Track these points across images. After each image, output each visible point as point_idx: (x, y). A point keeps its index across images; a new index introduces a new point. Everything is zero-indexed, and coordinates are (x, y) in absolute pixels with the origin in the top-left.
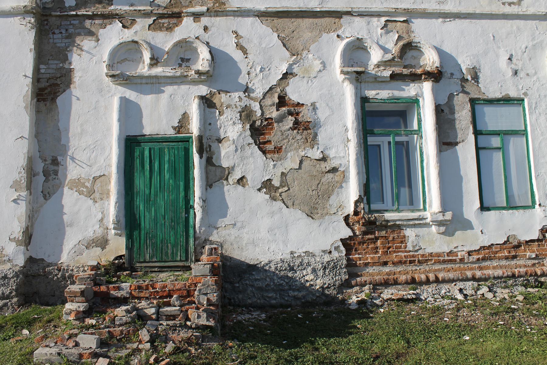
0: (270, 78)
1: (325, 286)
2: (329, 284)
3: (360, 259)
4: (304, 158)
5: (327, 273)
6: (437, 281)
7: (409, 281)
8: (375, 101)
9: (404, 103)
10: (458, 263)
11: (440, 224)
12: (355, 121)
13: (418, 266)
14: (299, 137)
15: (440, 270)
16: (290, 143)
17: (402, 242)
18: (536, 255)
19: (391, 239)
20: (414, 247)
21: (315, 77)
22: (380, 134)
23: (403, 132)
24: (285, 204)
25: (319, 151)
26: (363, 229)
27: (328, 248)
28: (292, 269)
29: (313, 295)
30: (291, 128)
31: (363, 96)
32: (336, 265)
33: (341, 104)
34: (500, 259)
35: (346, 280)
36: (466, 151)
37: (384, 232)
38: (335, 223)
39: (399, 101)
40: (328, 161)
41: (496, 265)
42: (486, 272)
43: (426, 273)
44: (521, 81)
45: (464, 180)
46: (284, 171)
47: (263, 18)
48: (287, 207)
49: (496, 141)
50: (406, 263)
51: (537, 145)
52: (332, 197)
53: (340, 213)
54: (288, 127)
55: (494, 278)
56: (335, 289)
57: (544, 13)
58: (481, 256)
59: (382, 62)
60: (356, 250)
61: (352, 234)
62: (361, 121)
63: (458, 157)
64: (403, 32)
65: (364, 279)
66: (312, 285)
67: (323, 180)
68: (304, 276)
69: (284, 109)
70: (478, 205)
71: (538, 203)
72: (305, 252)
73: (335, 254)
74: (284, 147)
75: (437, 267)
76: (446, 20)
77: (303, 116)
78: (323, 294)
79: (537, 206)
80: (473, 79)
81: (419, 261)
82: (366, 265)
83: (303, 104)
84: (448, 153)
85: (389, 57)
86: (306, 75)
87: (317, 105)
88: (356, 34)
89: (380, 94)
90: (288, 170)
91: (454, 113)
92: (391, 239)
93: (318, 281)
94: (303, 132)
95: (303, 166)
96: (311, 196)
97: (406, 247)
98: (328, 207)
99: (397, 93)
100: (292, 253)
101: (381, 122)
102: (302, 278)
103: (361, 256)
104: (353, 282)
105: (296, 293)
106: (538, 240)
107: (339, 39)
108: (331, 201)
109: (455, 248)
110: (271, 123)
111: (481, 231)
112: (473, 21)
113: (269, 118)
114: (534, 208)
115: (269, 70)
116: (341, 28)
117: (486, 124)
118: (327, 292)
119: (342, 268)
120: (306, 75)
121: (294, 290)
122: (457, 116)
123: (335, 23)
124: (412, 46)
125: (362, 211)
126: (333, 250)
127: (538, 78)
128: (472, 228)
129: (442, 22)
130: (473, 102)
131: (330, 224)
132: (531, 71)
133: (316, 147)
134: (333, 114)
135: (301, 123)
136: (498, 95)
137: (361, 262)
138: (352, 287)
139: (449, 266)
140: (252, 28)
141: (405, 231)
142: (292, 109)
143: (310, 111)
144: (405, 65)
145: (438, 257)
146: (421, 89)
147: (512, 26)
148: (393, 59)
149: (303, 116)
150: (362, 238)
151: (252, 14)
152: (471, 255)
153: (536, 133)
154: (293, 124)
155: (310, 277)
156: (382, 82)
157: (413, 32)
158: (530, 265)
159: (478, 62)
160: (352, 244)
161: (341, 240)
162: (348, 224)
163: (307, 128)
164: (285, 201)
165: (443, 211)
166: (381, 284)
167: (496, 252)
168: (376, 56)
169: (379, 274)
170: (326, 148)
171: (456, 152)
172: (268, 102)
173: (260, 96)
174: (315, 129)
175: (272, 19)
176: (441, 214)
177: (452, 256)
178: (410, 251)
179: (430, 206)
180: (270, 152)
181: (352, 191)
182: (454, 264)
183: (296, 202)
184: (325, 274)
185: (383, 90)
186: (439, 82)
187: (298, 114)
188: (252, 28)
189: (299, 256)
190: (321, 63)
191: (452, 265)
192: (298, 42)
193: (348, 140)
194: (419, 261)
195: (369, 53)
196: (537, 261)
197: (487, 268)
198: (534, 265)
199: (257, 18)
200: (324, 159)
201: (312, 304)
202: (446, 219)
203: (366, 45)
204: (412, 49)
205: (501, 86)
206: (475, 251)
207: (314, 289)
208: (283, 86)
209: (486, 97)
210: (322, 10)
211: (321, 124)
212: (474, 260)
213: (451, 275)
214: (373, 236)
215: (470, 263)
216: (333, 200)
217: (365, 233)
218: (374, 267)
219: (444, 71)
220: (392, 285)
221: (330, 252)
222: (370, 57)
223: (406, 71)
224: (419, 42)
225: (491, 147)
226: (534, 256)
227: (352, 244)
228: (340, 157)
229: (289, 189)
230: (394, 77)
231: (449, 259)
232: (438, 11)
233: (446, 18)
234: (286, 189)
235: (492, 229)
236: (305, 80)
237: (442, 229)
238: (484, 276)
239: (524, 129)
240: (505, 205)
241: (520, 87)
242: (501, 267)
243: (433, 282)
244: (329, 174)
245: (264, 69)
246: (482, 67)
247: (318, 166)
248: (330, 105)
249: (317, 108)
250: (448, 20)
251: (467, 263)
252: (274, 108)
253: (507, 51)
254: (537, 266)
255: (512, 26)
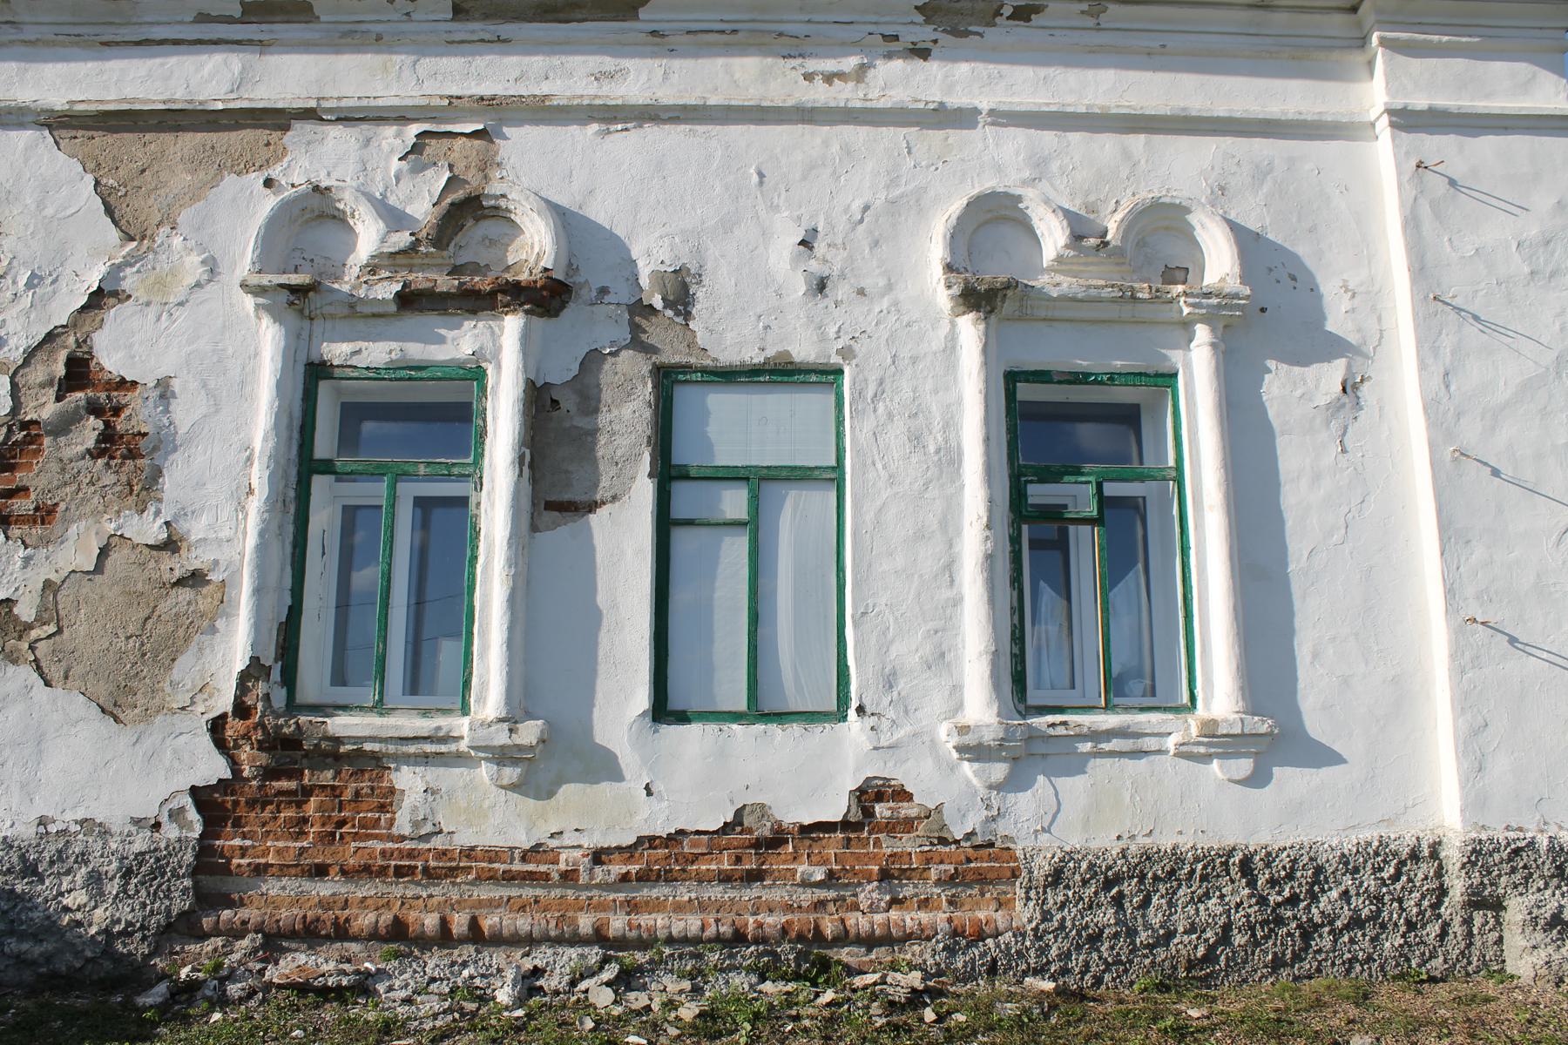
0: (54, 305)
1: (117, 929)
2: (129, 924)
3: (244, 851)
4: (114, 541)
5: (131, 889)
6: (475, 935)
7: (383, 931)
8: (350, 373)
9: (440, 379)
10: (554, 886)
11: (502, 756)
12: (272, 435)
13: (426, 887)
14: (109, 478)
15: (492, 904)
16: (81, 495)
17: (382, 808)
18: (831, 874)
19: (348, 795)
20: (416, 824)
21: (181, 304)
22: (352, 473)
23: (422, 470)
24: (42, 675)
25: (160, 521)
26: (263, 759)
27: (150, 812)
28: (30, 870)
29: (78, 954)
30: (88, 451)
31: (315, 358)
32: (162, 867)
33: (244, 385)
34: (701, 879)
35: (182, 914)
36: (622, 534)
37: (329, 774)
38: (183, 738)
39: (424, 374)
40: (183, 552)
41: (686, 898)
42: (645, 920)
43: (448, 911)
44: (836, 312)
45: (605, 622)
46: (53, 577)
47: (64, 133)
48: (48, 684)
49: (734, 502)
50: (386, 875)
51: (869, 517)
52: (181, 660)
53: (200, 708)
54: (80, 449)
55: (670, 940)
56: (144, 938)
57: (931, 106)
58: (634, 868)
59: (380, 255)
60: (237, 823)
61: (228, 775)
62: (296, 435)
63: (592, 549)
64: (467, 168)
65: (250, 914)
66: (79, 924)
67: (163, 607)
68: (61, 894)
69: (80, 395)
70: (642, 699)
71: (854, 704)
72: (82, 822)
73: (171, 832)
74: (62, 506)
75: (486, 892)
76: (613, 128)
77: (129, 418)
78: (108, 951)
79: (852, 713)
80: (668, 304)
81: (426, 870)
82: (260, 871)
83: (134, 383)
84: (561, 534)
85: (403, 239)
86: (157, 299)
87: (176, 385)
88: (323, 174)
89: (365, 353)
90: (64, 573)
91: (596, 410)
92: (348, 795)
93: (99, 912)
94: (122, 464)
95: (109, 563)
96: (122, 653)
97: (391, 822)
98: (168, 690)
99: (417, 351)
100: (42, 821)
101: (363, 442)
102: (55, 898)
103: (248, 843)
104: (207, 922)
105: (25, 946)
106: (845, 825)
107: (268, 191)
108: (176, 673)
109: (552, 836)
110: (38, 435)
111: (647, 788)
112: (700, 128)
113: (32, 422)
114: (844, 718)
115: (53, 283)
116: (281, 160)
117: (708, 447)
118: (120, 947)
119: (178, 877)
120: (157, 299)
121: (22, 936)
122: (603, 419)
123: (268, 144)
124: (483, 207)
125: (260, 706)
126: (164, 819)
127: (896, 303)
128: (616, 775)
129: (598, 133)
130: (667, 379)
131: (168, 741)
132: (873, 282)
133: (152, 509)
134: (217, 411)
135: (122, 437)
136: (752, 355)
137: (244, 861)
138: (203, 937)
139: (528, 892)
140: (26, 161)
141: (393, 776)
142: (103, 395)
143: (151, 403)
144: (455, 261)
145: (491, 861)
146: (495, 337)
147: (826, 143)
148: (413, 248)
149: (129, 418)
150: (260, 788)
151: (30, 119)
152: (602, 863)
153: (871, 475)
154: (98, 441)
155: (79, 898)
156: (374, 315)
157: (498, 165)
158: (805, 905)
159: (698, 251)
160: (229, 805)
161: (194, 791)
162: (220, 744)
163: (133, 454)
164: (43, 664)
165: (511, 720)
166: (293, 935)
167: (695, 858)
168: (369, 237)
169: (296, 902)
170: (183, 513)
171: (589, 529)
172: (37, 374)
173: (17, 356)
174: (156, 455)
175: (90, 133)
176: (505, 726)
177: (538, 863)
178: (402, 838)
179: (482, 699)
180: (22, 520)
181: (236, 643)
182: (543, 887)
183: (77, 670)
184: (125, 892)
185: (374, 341)
186: (556, 315)
187: (117, 411)
188: (26, 161)
189: (64, 832)
190: (203, 262)
191: (539, 892)
192: (150, 202)
193: (251, 492)
194: (426, 870)
195: (351, 230)
196: (832, 894)
197: (655, 906)
198: (820, 905)
199: (47, 133)
200: (171, 545)
201: (66, 982)
202: (518, 741)
203: (341, 206)
204: (485, 217)
205: (767, 327)
206: (619, 848)
207: (81, 937)
208: (86, 328)
209: (708, 362)
210: (231, 106)
211: (178, 443)
212: (612, 878)
213: (523, 924)
214: (293, 785)
215: (598, 886)
216: (185, 670)
217: (269, 773)
218: (285, 880)
219: (582, 280)
220: (328, 937)
221: (157, 826)
222: (355, 244)
223: (446, 284)
224: (503, 196)
225: (720, 518)
226: (819, 875)
227: (229, 805)
228: (219, 541)
229: (60, 631)
230: (409, 300)
231: (530, 867)
232: (586, 102)
233: (614, 120)
234: (52, 629)
235: (687, 781)
236: (152, 312)
237: (511, 774)
238: (634, 933)
239: (834, 463)
240: (742, 706)
241: (832, 331)
242: (702, 907)
243: (463, 940)
244: (180, 590)
245: (41, 278)
246: (709, 266)
247: (152, 564)
248: (212, 385)
249: (174, 395)
250: (619, 127)
251: (588, 887)
252: (51, 392)
253: (799, 218)
254: (831, 907)
255: (826, 143)
